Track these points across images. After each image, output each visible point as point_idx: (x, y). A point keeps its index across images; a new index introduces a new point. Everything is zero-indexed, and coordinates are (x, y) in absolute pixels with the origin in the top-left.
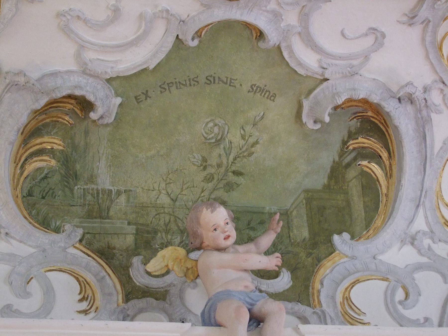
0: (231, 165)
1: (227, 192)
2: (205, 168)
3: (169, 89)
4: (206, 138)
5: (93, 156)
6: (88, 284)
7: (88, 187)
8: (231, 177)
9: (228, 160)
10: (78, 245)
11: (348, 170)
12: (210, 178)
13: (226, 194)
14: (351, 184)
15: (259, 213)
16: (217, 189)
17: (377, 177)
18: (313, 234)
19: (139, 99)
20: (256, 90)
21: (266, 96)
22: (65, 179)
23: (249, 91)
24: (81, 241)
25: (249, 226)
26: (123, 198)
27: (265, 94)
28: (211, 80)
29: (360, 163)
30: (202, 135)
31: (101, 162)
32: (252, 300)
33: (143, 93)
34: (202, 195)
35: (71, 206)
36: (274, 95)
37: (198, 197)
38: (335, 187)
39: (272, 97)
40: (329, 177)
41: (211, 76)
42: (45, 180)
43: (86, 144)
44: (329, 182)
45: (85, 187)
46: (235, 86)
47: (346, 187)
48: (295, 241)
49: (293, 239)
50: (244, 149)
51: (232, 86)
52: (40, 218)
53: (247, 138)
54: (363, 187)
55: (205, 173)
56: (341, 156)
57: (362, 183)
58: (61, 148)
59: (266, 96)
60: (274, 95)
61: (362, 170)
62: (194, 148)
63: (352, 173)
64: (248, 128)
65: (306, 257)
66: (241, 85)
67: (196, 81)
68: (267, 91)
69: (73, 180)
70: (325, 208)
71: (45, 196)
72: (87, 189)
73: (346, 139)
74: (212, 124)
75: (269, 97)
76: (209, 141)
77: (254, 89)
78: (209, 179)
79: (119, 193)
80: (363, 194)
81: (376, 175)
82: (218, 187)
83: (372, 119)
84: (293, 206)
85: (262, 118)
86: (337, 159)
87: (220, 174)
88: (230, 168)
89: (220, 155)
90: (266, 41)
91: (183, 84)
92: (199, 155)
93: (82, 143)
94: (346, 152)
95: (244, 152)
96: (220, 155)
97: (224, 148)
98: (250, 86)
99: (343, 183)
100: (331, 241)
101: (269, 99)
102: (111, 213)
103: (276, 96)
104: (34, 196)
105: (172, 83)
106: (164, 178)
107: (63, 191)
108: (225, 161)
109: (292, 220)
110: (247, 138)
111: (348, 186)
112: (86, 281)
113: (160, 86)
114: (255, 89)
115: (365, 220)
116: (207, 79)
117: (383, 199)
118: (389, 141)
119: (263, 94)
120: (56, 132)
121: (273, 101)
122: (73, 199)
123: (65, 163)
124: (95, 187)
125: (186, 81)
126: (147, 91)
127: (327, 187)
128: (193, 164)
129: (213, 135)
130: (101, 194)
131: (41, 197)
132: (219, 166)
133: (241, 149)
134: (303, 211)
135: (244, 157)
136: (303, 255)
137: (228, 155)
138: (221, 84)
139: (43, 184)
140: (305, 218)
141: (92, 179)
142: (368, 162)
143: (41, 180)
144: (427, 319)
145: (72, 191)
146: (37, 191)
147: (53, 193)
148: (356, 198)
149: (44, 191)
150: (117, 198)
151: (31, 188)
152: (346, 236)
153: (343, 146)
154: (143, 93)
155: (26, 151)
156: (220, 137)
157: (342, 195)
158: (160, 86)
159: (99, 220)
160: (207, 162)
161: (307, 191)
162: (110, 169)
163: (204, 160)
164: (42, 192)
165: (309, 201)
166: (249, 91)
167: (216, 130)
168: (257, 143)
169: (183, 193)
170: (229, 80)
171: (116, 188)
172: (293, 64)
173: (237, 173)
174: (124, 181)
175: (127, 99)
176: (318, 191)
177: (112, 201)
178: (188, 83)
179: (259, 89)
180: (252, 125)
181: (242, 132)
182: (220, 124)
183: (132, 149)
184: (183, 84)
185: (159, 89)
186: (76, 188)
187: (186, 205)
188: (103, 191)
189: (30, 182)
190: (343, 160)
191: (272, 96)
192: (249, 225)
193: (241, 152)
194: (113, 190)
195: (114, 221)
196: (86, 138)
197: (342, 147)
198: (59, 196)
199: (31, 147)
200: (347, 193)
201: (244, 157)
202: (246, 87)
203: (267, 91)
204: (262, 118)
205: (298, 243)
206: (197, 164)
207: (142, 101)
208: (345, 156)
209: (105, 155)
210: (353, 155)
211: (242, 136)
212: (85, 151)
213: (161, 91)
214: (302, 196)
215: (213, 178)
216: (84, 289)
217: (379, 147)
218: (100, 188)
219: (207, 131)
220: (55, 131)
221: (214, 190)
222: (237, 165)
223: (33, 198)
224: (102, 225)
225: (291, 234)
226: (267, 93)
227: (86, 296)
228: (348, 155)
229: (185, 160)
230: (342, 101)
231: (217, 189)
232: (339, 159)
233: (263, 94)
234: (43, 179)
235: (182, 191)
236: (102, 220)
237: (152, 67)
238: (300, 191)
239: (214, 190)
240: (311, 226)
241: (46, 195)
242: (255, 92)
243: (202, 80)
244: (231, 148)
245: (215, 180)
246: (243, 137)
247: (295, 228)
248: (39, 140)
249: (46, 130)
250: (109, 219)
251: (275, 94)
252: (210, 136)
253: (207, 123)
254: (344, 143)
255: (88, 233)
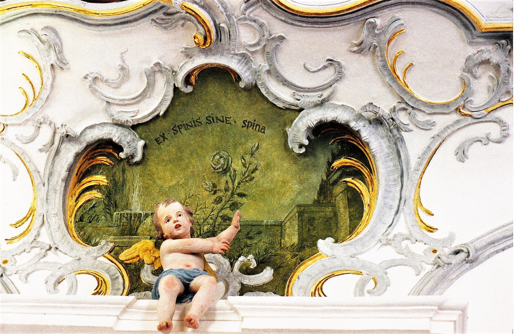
0: (236, 189)
1: (232, 211)
2: (215, 193)
3: (180, 130)
4: (214, 168)
5: (129, 189)
6: (105, 283)
7: (124, 212)
8: (237, 199)
9: (233, 184)
10: (107, 255)
11: (335, 186)
12: (219, 200)
13: (231, 212)
14: (337, 198)
15: (258, 225)
16: (225, 208)
17: (361, 191)
18: (302, 240)
19: (159, 141)
20: (248, 125)
21: (257, 129)
22: (107, 207)
23: (243, 127)
24: (110, 252)
25: (247, 236)
26: (149, 220)
27: (256, 128)
28: (210, 120)
29: (345, 180)
30: (211, 166)
31: (135, 193)
32: (189, 275)
33: (161, 136)
34: (212, 213)
35: (110, 227)
36: (263, 128)
37: (208, 215)
38: (324, 202)
39: (262, 130)
40: (318, 194)
41: (210, 117)
42: (93, 209)
43: (124, 180)
44: (318, 197)
45: (122, 212)
46: (230, 124)
47: (334, 201)
48: (285, 246)
49: (283, 245)
50: (246, 175)
51: (229, 123)
52: (85, 237)
53: (247, 166)
54: (348, 199)
55: (214, 197)
56: (327, 176)
57: (348, 197)
58: (106, 184)
59: (257, 129)
60: (263, 128)
61: (348, 186)
62: (206, 177)
63: (338, 189)
64: (247, 158)
65: (291, 258)
66: (235, 122)
67: (199, 122)
68: (257, 125)
69: (113, 208)
70: (314, 219)
71: (92, 221)
72: (123, 214)
73: (330, 161)
74: (218, 157)
75: (260, 130)
76: (217, 171)
77: (247, 124)
78: (218, 201)
79: (147, 215)
80: (349, 205)
81: (359, 189)
82: (225, 206)
83: (350, 141)
84: (288, 218)
85: (258, 148)
86: (325, 178)
87: (227, 196)
88: (235, 191)
89: (227, 182)
90: (242, 80)
91: (190, 126)
92: (210, 182)
93: (121, 179)
94: (332, 172)
95: (246, 178)
96: (227, 182)
97: (230, 175)
98: (242, 122)
99: (331, 197)
100: (316, 245)
101: (260, 132)
102: (139, 231)
103: (265, 128)
104: (84, 221)
105: (181, 125)
106: (183, 203)
107: (105, 216)
108: (231, 186)
109: (285, 230)
110: (247, 166)
111: (335, 200)
112: (104, 280)
113: (173, 129)
114: (247, 124)
115: (350, 227)
116: (208, 120)
117: (366, 209)
118: (369, 159)
119: (255, 128)
120: (102, 172)
121: (264, 132)
122: (111, 222)
123: (109, 195)
124: (129, 212)
125: (191, 122)
126: (163, 134)
127: (317, 203)
128: (206, 190)
129: (220, 165)
130: (133, 217)
131: (88, 221)
132: (226, 190)
133: (243, 176)
134: (296, 222)
135: (246, 181)
136: (289, 256)
137: (233, 181)
138: (220, 123)
139: (91, 212)
140: (296, 228)
141: (127, 206)
142: (352, 179)
143: (90, 209)
144: (5, 162)
145: (111, 215)
146: (86, 219)
147: (98, 218)
148: (342, 210)
149: (92, 216)
150: (145, 220)
151: (82, 215)
152: (330, 240)
153: (329, 167)
154: (161, 136)
155: (80, 187)
156: (225, 167)
157: (330, 208)
158: (173, 129)
159: (128, 236)
160: (216, 188)
161: (299, 206)
162: (142, 198)
163: (214, 186)
164: (90, 217)
165: (301, 214)
166: (243, 127)
167: (222, 161)
168: (256, 169)
169: (197, 213)
170: (224, 118)
171: (145, 212)
172: (271, 99)
173: (241, 195)
174: (151, 206)
175: (150, 142)
176: (309, 206)
177: (140, 222)
178: (193, 124)
179: (250, 123)
180: (250, 155)
181: (243, 161)
182: (225, 156)
183: (158, 181)
184: (190, 126)
185: (173, 131)
186: (115, 213)
187: (198, 222)
188: (135, 214)
189: (82, 211)
190: (330, 179)
191: (261, 129)
192: (248, 234)
193: (244, 177)
194: (143, 214)
195: (140, 236)
196: (123, 175)
197: (328, 167)
198: (102, 220)
199: (83, 184)
200: (335, 206)
201: (246, 181)
202: (240, 123)
203: (257, 125)
204: (258, 148)
205: (287, 248)
206: (209, 189)
207: (161, 142)
208: (332, 175)
209: (138, 187)
210: (338, 173)
211: (243, 165)
212: (123, 186)
213: (174, 133)
214: (295, 210)
215: (222, 200)
216: (100, 286)
217: (360, 165)
218: (132, 213)
219: (215, 163)
220: (100, 172)
221: (222, 209)
222: (241, 188)
223: (83, 222)
224: (130, 240)
225: (282, 241)
226: (258, 127)
227: (100, 291)
228: (334, 174)
229: (199, 187)
230: (314, 124)
231: (225, 208)
232: (327, 179)
233: (255, 128)
234: (92, 208)
235: (196, 212)
236: (131, 236)
237: (161, 114)
238: (293, 206)
239: (222, 209)
240: (300, 234)
241: (93, 220)
242: (248, 126)
243: (204, 120)
244: (235, 175)
245: (223, 202)
246: (244, 165)
247: (286, 236)
248: (89, 179)
249: (94, 172)
250: (136, 235)
251: (264, 127)
252: (218, 167)
253: (214, 156)
254: (330, 164)
255: (117, 246)
